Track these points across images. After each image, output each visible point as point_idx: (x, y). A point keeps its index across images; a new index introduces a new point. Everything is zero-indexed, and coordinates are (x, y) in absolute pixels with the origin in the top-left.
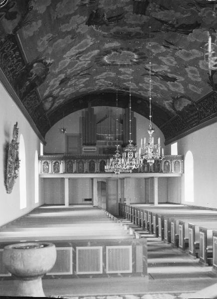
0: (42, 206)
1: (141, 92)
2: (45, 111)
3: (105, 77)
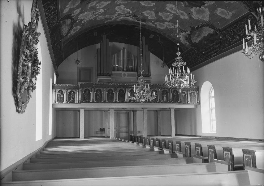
0: (56, 138)
2: (62, 37)
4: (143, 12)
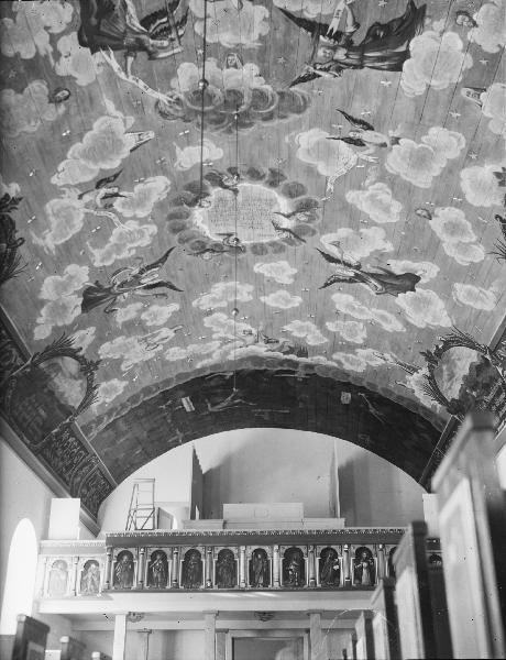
1: (338, 356)
3: (224, 304)
4: (285, 327)
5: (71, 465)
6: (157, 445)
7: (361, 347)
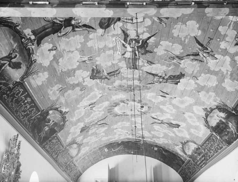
3: (121, 127)
5: (71, 171)
6: (96, 160)
7: (162, 138)
